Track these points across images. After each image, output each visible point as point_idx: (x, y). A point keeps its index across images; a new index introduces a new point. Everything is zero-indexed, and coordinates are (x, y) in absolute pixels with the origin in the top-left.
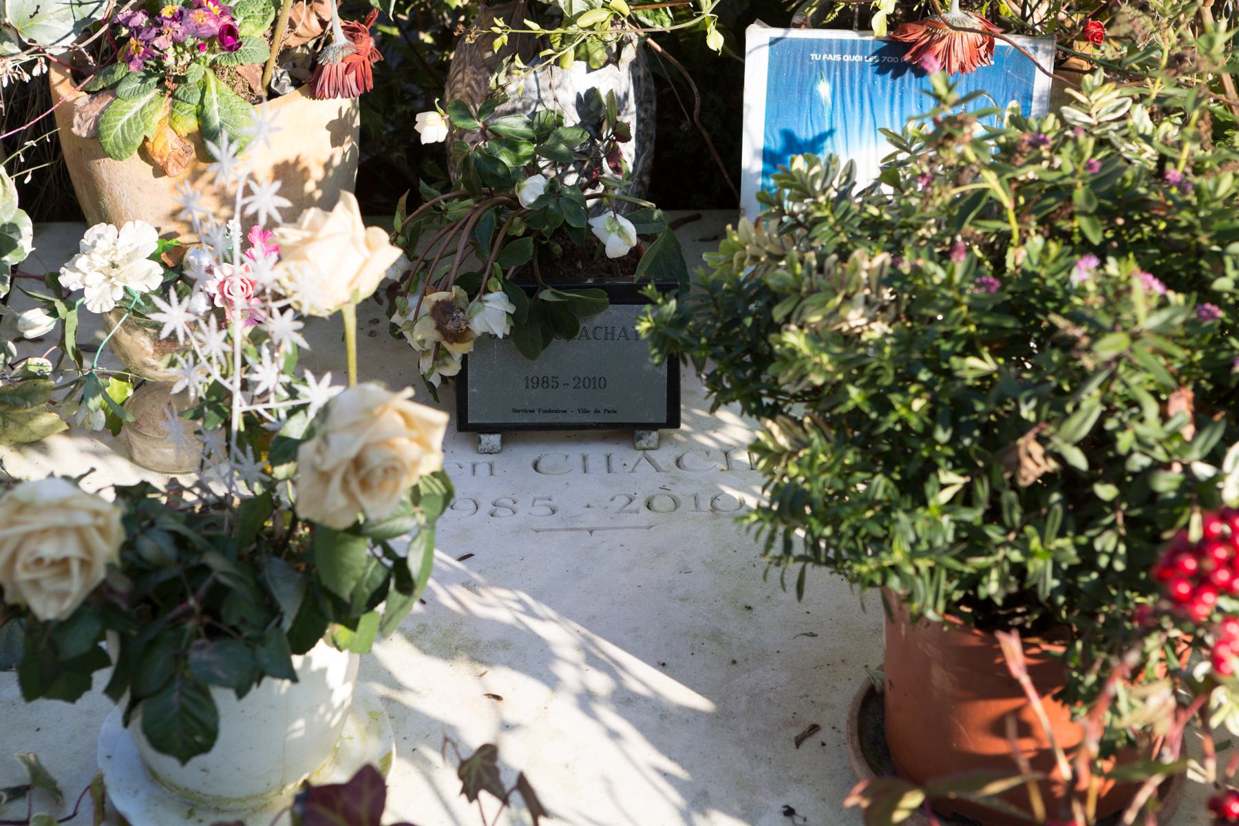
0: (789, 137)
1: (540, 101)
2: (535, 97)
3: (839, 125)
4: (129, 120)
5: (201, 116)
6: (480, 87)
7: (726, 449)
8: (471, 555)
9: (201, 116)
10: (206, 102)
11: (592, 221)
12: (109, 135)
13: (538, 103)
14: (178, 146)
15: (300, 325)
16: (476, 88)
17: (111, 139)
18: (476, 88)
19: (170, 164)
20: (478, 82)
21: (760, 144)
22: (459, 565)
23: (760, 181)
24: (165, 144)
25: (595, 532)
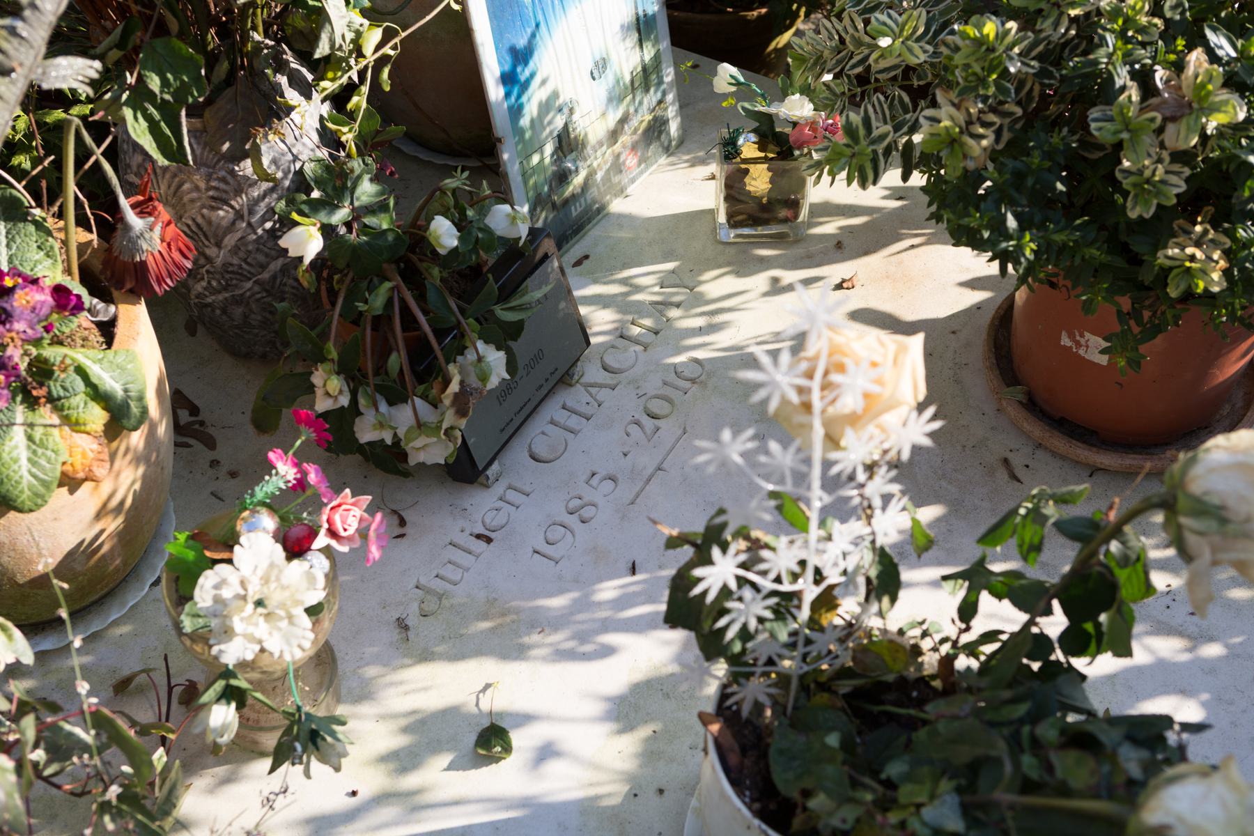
0: (513, 51)
1: (296, 158)
2: (290, 157)
3: (540, 18)
4: (29, 460)
5: (98, 395)
6: (227, 183)
7: (618, 333)
8: (634, 564)
9: (98, 395)
10: (94, 380)
11: (283, 243)
12: (22, 492)
13: (294, 162)
14: (95, 446)
15: (894, 473)
16: (222, 186)
17: (27, 492)
18: (222, 186)
19: (94, 469)
20: (223, 180)
21: (498, 74)
22: (638, 577)
23: (506, 105)
24: (84, 455)
25: (664, 466)
